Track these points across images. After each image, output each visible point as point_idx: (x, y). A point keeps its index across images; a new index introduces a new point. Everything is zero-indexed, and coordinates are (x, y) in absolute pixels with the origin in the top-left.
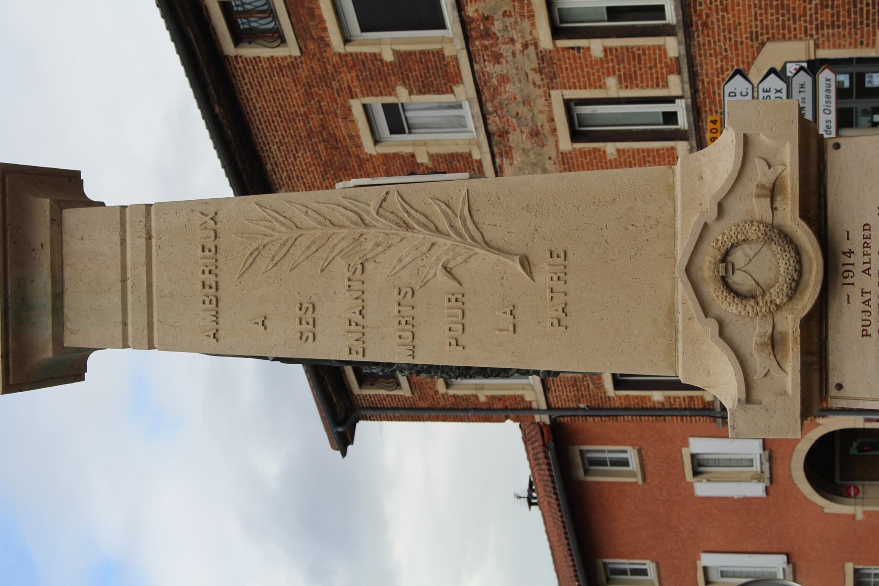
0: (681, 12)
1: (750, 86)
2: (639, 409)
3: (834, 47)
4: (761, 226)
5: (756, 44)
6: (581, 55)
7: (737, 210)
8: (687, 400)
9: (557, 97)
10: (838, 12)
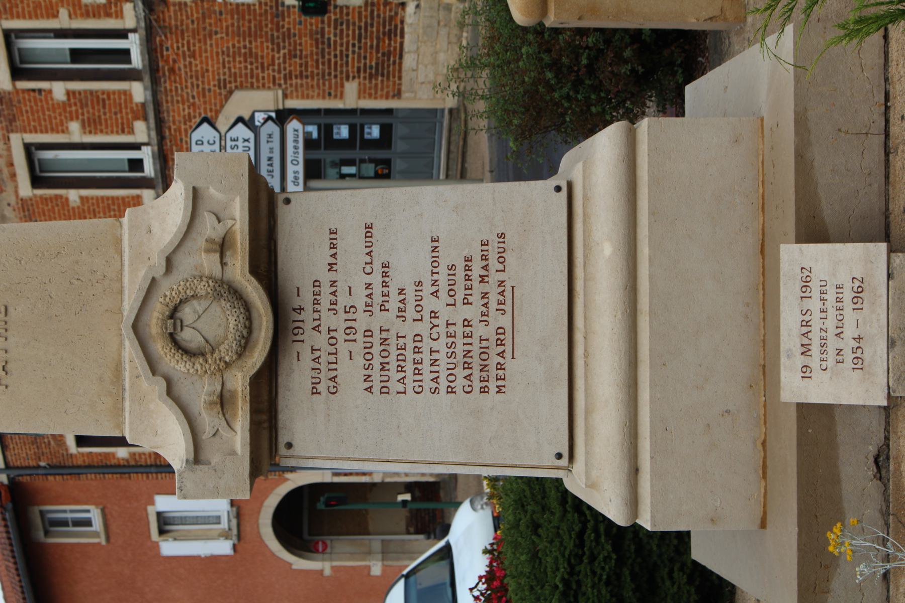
0: (147, 56)
1: (217, 135)
2: (102, 467)
3: (303, 97)
4: (210, 282)
5: (224, 92)
6: (43, 98)
7: (186, 265)
8: (153, 457)
9: (17, 141)
10: (307, 63)
